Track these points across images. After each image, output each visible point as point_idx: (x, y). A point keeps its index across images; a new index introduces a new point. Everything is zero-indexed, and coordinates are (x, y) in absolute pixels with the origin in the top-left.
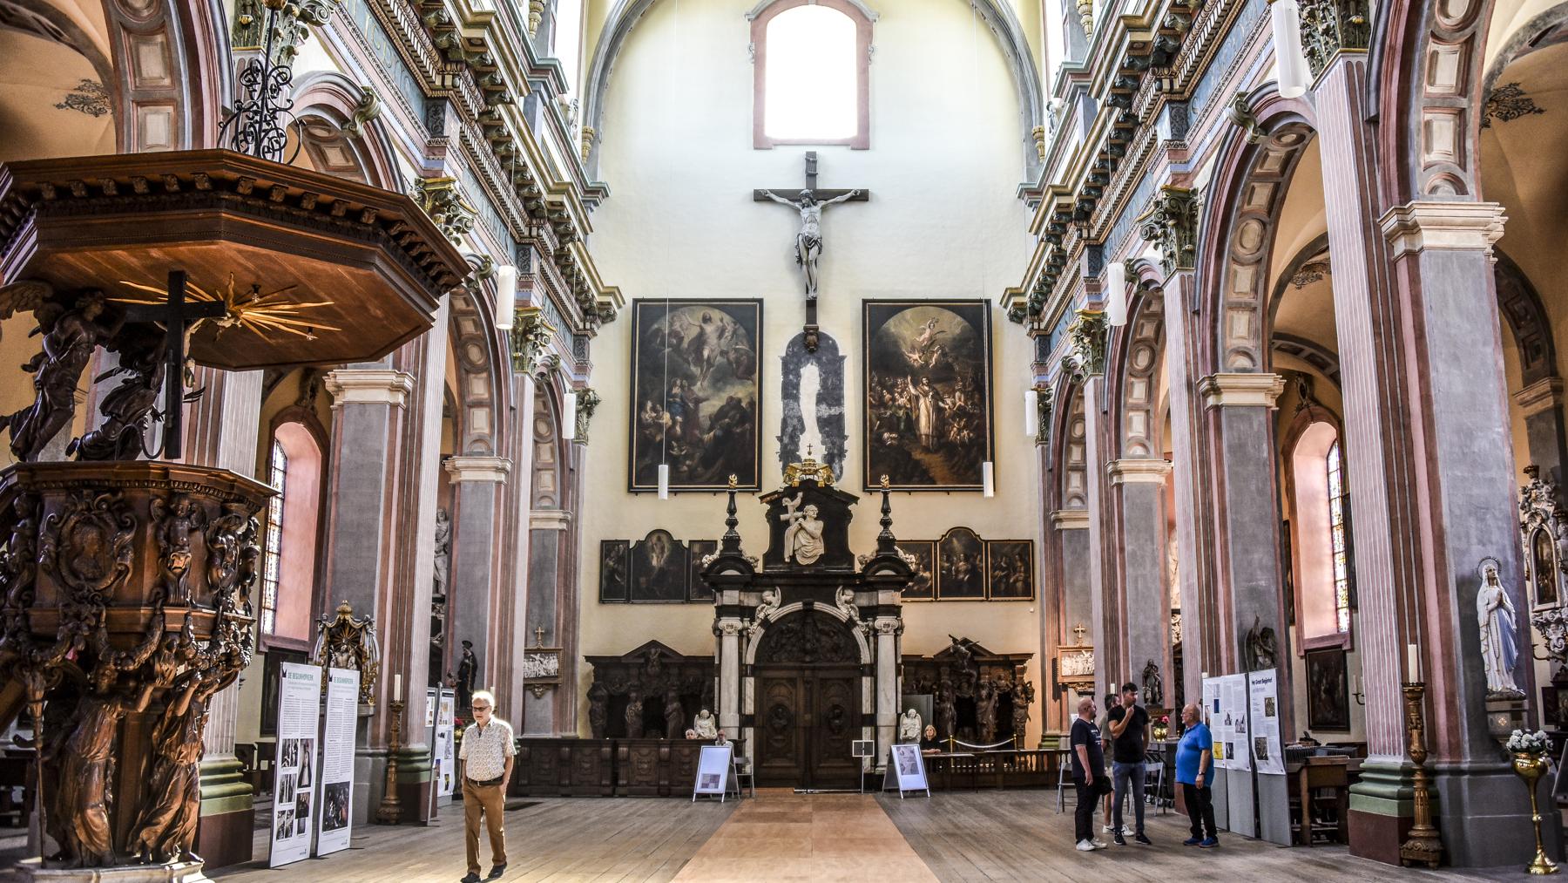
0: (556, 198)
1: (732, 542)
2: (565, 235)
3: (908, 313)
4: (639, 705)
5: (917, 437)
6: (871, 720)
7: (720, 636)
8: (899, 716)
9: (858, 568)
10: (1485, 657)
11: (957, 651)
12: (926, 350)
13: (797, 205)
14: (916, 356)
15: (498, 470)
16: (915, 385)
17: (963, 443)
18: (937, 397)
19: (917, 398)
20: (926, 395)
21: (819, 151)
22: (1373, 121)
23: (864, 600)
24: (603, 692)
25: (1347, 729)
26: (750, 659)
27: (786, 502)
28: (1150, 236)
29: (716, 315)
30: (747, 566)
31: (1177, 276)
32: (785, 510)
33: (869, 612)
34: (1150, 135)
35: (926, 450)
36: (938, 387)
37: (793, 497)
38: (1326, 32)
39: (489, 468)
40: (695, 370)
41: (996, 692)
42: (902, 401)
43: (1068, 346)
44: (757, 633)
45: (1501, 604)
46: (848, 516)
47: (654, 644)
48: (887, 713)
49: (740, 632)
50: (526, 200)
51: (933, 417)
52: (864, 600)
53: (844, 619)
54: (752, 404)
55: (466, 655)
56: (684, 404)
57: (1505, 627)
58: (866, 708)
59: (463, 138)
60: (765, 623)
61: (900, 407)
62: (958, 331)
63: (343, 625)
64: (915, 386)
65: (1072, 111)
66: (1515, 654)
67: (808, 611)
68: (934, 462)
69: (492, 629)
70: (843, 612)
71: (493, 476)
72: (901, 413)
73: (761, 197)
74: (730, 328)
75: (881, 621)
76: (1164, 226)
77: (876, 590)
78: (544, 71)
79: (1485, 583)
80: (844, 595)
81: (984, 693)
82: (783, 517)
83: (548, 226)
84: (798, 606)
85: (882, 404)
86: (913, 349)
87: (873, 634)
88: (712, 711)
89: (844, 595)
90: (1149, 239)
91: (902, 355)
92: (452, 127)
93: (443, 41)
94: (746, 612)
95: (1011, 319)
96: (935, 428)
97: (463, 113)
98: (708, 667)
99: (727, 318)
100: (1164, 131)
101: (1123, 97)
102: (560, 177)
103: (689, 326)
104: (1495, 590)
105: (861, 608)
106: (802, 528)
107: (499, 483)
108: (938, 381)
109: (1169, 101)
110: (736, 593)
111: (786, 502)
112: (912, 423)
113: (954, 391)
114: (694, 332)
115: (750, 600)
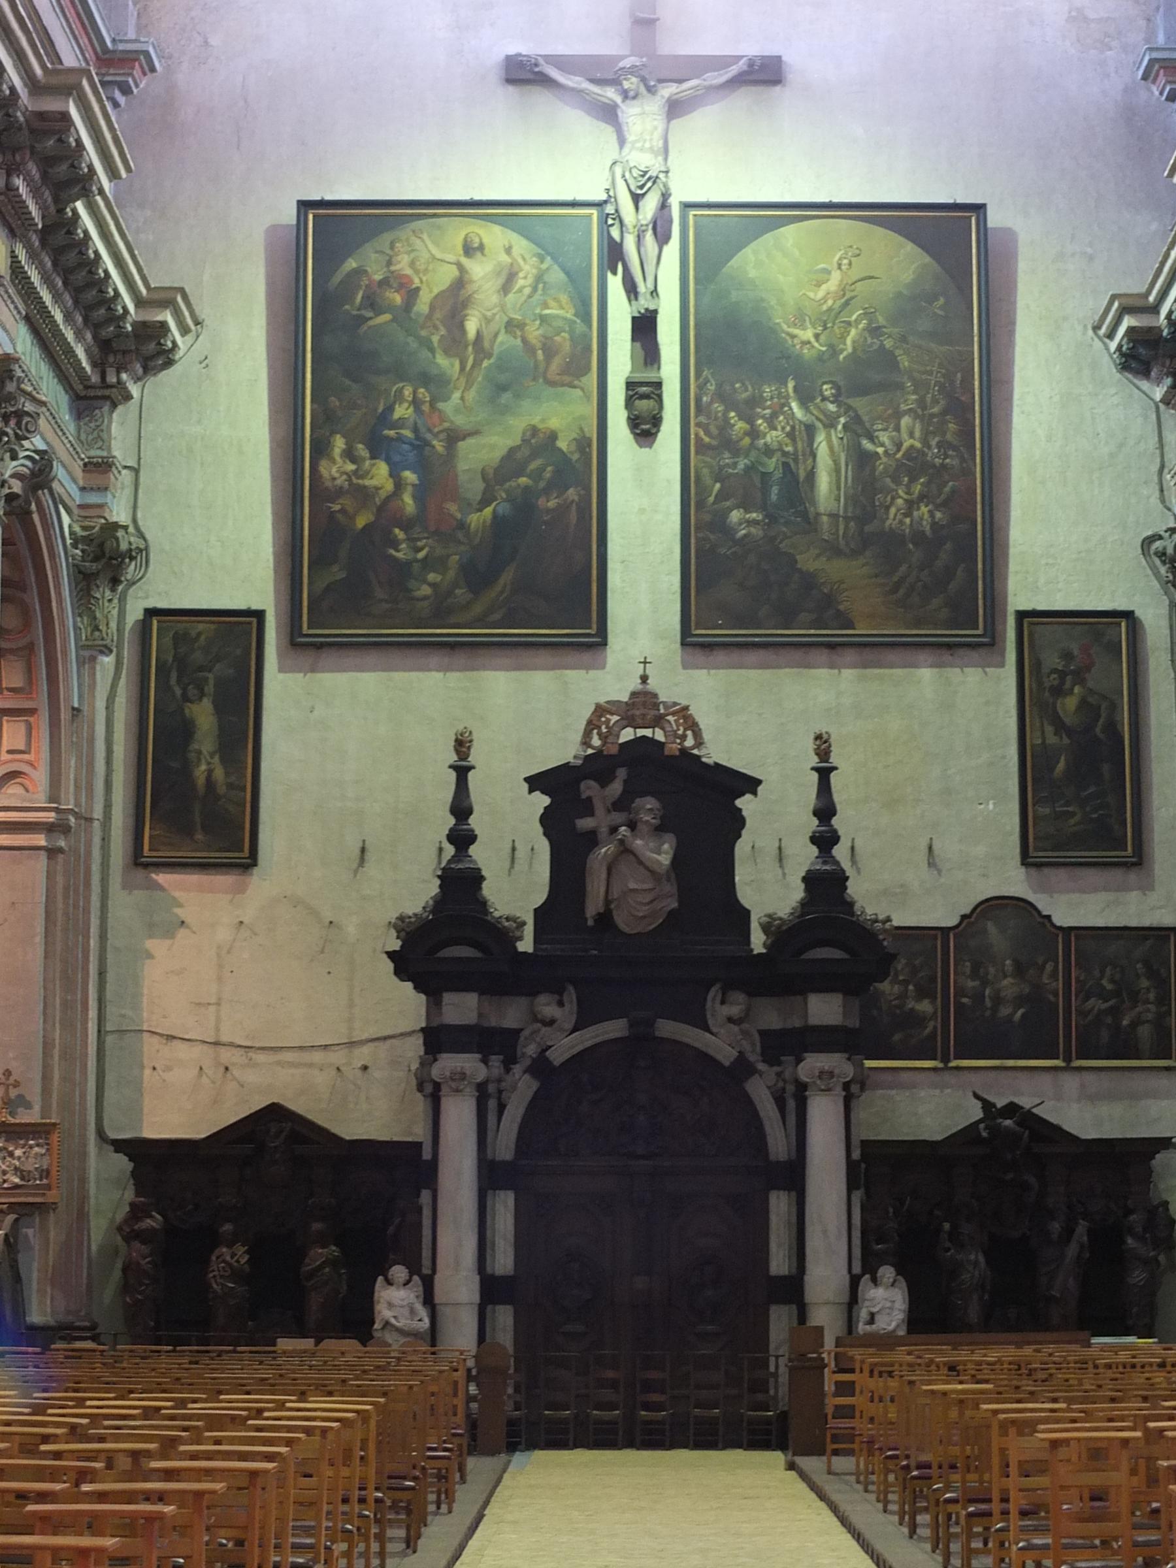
0: (51, 105)
1: (460, 884)
2: (67, 179)
3: (790, 234)
5: (809, 523)
6: (792, 1289)
8: (855, 1282)
9: (758, 941)
11: (995, 1131)
12: (826, 321)
13: (611, 94)
14: (808, 334)
16: (805, 399)
17: (918, 537)
18: (857, 428)
19: (810, 430)
20: (830, 424)
26: (505, 1147)
27: (589, 788)
29: (494, 236)
30: (500, 935)
32: (588, 808)
33: (787, 1045)
35: (833, 550)
37: (604, 779)
40: (445, 363)
41: (1082, 1228)
42: (773, 437)
44: (523, 1089)
46: (737, 822)
47: (274, 1112)
48: (826, 1276)
49: (481, 1088)
51: (847, 473)
52: (771, 1016)
56: (421, 444)
58: (779, 1264)
60: (541, 1067)
61: (768, 451)
62: (907, 276)
67: (641, 1039)
68: (851, 578)
70: (721, 1045)
72: (772, 464)
75: (813, 1064)
77: (803, 992)
80: (723, 1009)
81: (1056, 1227)
82: (585, 823)
83: (33, 169)
84: (614, 1029)
85: (727, 444)
86: (800, 319)
87: (793, 1101)
88: (414, 1268)
89: (723, 1009)
95: (1124, 367)
96: (852, 500)
98: (404, 1169)
99: (521, 245)
105: (763, 1034)
106: (625, 850)
108: (862, 390)
110: (471, 1000)
111: (589, 788)
112: (797, 483)
113: (898, 415)
114: (444, 277)
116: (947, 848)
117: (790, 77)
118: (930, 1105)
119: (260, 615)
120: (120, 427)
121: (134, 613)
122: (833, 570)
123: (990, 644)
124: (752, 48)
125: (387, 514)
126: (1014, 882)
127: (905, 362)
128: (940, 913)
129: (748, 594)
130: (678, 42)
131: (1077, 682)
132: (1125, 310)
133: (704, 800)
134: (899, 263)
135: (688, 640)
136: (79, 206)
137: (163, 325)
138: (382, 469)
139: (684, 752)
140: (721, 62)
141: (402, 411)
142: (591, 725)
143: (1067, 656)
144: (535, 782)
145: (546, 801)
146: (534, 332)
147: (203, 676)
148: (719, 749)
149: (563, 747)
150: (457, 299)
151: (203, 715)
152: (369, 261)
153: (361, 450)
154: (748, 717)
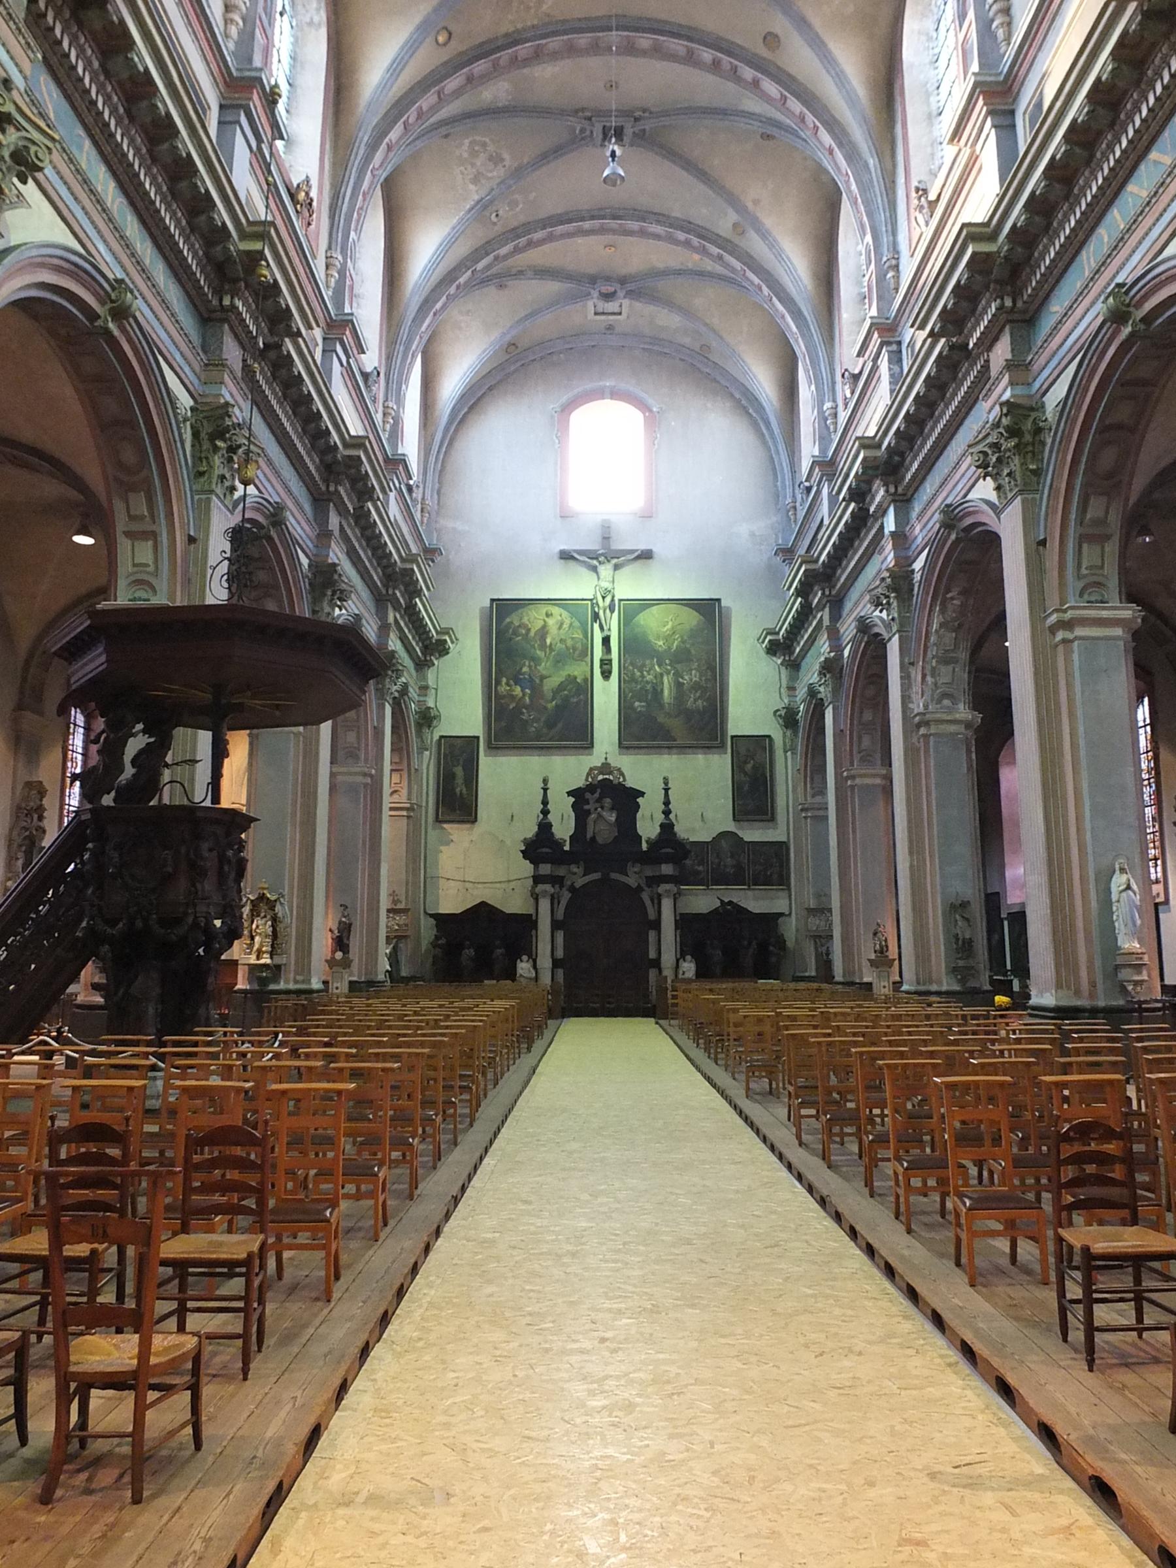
0: (408, 566)
1: (545, 827)
2: (413, 591)
4: (472, 952)
5: (661, 706)
7: (537, 900)
8: (678, 961)
9: (644, 846)
10: (1116, 924)
12: (667, 638)
13: (595, 562)
14: (661, 643)
15: (365, 775)
18: (678, 675)
19: (662, 675)
20: (668, 673)
22: (1043, 543)
23: (649, 872)
24: (442, 941)
26: (560, 916)
27: (588, 795)
28: (877, 604)
29: (556, 610)
30: (559, 844)
31: (897, 636)
34: (877, 526)
35: (669, 715)
36: (679, 666)
38: (1009, 475)
39: (356, 774)
42: (649, 678)
43: (811, 674)
44: (566, 896)
45: (1129, 887)
48: (668, 958)
50: (384, 568)
52: (649, 872)
53: (634, 884)
56: (531, 680)
58: (652, 955)
59: (246, 367)
60: (572, 889)
61: (647, 682)
63: (262, 897)
64: (659, 666)
65: (875, 368)
66: (1139, 922)
67: (605, 880)
69: (362, 895)
70: (632, 881)
71: (360, 779)
72: (649, 687)
75: (663, 888)
76: (887, 597)
78: (397, 463)
79: (1118, 872)
80: (633, 869)
82: (586, 807)
84: (596, 876)
86: (658, 638)
87: (657, 900)
88: (530, 957)
90: (877, 606)
91: (650, 642)
92: (334, 521)
93: (329, 458)
94: (556, 880)
97: (342, 511)
98: (527, 923)
99: (565, 614)
100: (890, 523)
101: (953, 323)
102: (410, 550)
103: (534, 619)
104: (1124, 878)
107: (366, 785)
109: (894, 501)
111: (588, 795)
112: (657, 692)
114: (540, 624)
115: (561, 871)
116: (709, 815)
117: (655, 556)
119: (478, 738)
120: (431, 675)
123: (722, 747)
124: (642, 546)
125: (520, 705)
126: (731, 826)
127: (693, 652)
129: (640, 730)
130: (618, 545)
133: (626, 799)
134: (692, 619)
138: (518, 689)
140: (632, 551)
141: (525, 669)
142: (588, 774)
144: (569, 793)
146: (569, 643)
147: (459, 759)
149: (580, 783)
150: (543, 632)
151: (459, 771)
152: (514, 619)
153: (512, 682)
154: (641, 771)
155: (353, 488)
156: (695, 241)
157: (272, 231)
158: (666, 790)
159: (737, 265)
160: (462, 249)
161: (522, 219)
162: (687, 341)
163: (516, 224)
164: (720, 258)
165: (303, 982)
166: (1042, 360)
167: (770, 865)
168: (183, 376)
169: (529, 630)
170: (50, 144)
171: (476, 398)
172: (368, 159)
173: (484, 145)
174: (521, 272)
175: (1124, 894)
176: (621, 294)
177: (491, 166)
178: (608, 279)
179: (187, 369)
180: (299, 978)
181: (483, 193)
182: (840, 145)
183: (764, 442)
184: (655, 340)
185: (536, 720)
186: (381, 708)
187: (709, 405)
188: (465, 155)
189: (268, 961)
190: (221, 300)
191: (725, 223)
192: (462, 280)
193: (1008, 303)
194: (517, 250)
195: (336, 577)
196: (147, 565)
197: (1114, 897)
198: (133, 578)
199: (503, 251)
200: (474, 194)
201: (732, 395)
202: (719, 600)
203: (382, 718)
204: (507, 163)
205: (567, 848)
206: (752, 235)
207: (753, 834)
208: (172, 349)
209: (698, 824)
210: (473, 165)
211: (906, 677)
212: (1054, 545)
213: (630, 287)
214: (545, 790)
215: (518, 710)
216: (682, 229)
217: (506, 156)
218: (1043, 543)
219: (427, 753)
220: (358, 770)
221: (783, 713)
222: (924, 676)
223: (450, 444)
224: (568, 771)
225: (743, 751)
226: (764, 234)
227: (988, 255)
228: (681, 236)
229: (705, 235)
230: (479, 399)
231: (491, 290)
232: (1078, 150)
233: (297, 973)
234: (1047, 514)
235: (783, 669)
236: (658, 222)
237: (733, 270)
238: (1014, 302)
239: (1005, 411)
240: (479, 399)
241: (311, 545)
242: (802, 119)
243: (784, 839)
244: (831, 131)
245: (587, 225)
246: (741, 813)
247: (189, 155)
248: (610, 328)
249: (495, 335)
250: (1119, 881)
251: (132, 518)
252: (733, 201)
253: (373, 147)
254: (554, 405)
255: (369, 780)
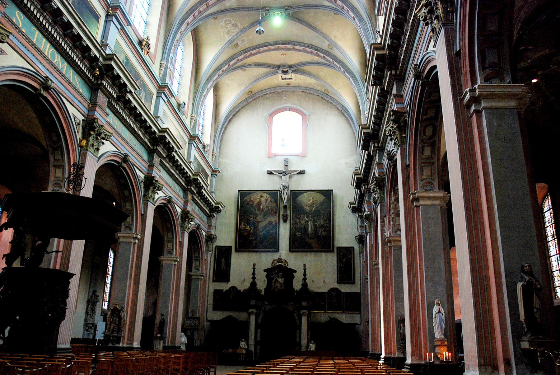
0: (217, 206)
1: (253, 284)
3: (305, 194)
5: (308, 234)
12: (311, 206)
13: (281, 175)
18: (314, 221)
19: (308, 222)
20: (311, 221)
21: (289, 158)
22: (408, 166)
25: (231, 247)
29: (265, 195)
30: (260, 291)
35: (311, 238)
36: (315, 218)
37: (275, 271)
40: (258, 212)
42: (303, 222)
45: (439, 312)
46: (293, 277)
48: (304, 341)
54: (276, 223)
55: (162, 318)
56: (254, 223)
57: (441, 319)
73: (270, 173)
74: (269, 199)
85: (296, 223)
86: (307, 206)
99: (268, 196)
103: (256, 198)
106: (278, 281)
109: (378, 150)
112: (306, 229)
114: (258, 200)
116: (326, 280)
117: (306, 172)
118: (323, 317)
119: (231, 247)
120: (213, 221)
121: (214, 247)
122: (311, 241)
123: (332, 251)
124: (301, 169)
125: (249, 232)
126: (336, 286)
127: (321, 212)
128: (325, 290)
129: (299, 244)
130: (292, 168)
131: (345, 258)
132: (351, 204)
133: (289, 273)
134: (321, 198)
135: (290, 251)
136: (203, 190)
137: (219, 207)
138: (248, 227)
139: (286, 267)
140: (297, 171)
141: (252, 219)
142: (273, 263)
143: (344, 253)
144: (265, 271)
145: (266, 273)
146: (270, 208)
147: (223, 254)
148: (291, 266)
149: (269, 266)
150: (260, 203)
151: (223, 261)
152: (247, 198)
153: (246, 224)
154: (295, 261)
155: (164, 147)
156: (314, 52)
157: (115, 57)
158: (305, 270)
159: (331, 60)
160: (224, 57)
161: (247, 46)
162: (319, 88)
163: (245, 48)
164: (324, 57)
165: (130, 344)
166: (405, 94)
167: (354, 303)
168: (79, 109)
169: (253, 202)
170: (8, 34)
171: (234, 113)
172: (178, 29)
173: (230, 21)
174: (250, 65)
175: (438, 315)
176: (290, 71)
177: (233, 28)
178: (284, 66)
179: (81, 106)
180: (129, 342)
181: (230, 37)
182: (357, 16)
183: (351, 127)
184: (306, 88)
185: (255, 240)
186: (183, 234)
187: (329, 113)
188: (224, 25)
189: (116, 335)
190: (97, 81)
191: (324, 45)
192: (224, 69)
193: (393, 72)
194: (246, 57)
195: (154, 181)
196: (59, 177)
197: (434, 316)
198: (54, 182)
199: (240, 58)
200: (227, 38)
201: (338, 109)
202: (332, 190)
203: (183, 237)
204: (239, 27)
205: (263, 293)
206: (334, 48)
207: (345, 288)
208: (74, 99)
209: (322, 284)
210: (227, 28)
211: (383, 222)
212: (412, 166)
213: (294, 69)
214: (254, 269)
215: (248, 236)
216: (308, 47)
217: (238, 24)
218: (408, 166)
219: (210, 253)
220: (172, 259)
221: (358, 238)
222: (389, 221)
223: (225, 129)
224: (266, 260)
225: (342, 254)
226: (339, 49)
227: (383, 55)
228: (309, 50)
229: (317, 49)
230: (237, 112)
231: (240, 71)
232: (400, 16)
233: (128, 340)
234: (409, 154)
235: (359, 219)
236: (300, 45)
237: (330, 62)
238: (396, 72)
239: (392, 113)
240: (237, 112)
241: (145, 170)
242: (343, 7)
243: (358, 291)
244: (353, 11)
245: (273, 47)
246: (340, 280)
247: (78, 34)
248: (288, 84)
249: (243, 87)
250: (436, 309)
251: (56, 160)
252: (326, 37)
253: (181, 24)
254: (266, 114)
255: (176, 263)
